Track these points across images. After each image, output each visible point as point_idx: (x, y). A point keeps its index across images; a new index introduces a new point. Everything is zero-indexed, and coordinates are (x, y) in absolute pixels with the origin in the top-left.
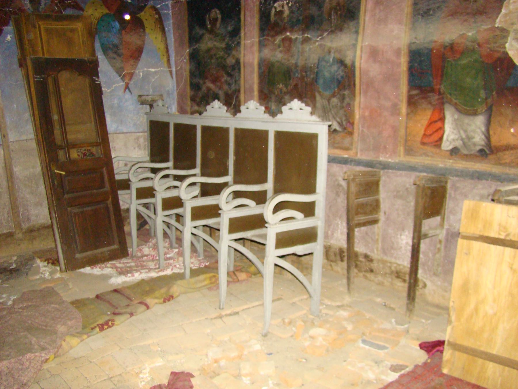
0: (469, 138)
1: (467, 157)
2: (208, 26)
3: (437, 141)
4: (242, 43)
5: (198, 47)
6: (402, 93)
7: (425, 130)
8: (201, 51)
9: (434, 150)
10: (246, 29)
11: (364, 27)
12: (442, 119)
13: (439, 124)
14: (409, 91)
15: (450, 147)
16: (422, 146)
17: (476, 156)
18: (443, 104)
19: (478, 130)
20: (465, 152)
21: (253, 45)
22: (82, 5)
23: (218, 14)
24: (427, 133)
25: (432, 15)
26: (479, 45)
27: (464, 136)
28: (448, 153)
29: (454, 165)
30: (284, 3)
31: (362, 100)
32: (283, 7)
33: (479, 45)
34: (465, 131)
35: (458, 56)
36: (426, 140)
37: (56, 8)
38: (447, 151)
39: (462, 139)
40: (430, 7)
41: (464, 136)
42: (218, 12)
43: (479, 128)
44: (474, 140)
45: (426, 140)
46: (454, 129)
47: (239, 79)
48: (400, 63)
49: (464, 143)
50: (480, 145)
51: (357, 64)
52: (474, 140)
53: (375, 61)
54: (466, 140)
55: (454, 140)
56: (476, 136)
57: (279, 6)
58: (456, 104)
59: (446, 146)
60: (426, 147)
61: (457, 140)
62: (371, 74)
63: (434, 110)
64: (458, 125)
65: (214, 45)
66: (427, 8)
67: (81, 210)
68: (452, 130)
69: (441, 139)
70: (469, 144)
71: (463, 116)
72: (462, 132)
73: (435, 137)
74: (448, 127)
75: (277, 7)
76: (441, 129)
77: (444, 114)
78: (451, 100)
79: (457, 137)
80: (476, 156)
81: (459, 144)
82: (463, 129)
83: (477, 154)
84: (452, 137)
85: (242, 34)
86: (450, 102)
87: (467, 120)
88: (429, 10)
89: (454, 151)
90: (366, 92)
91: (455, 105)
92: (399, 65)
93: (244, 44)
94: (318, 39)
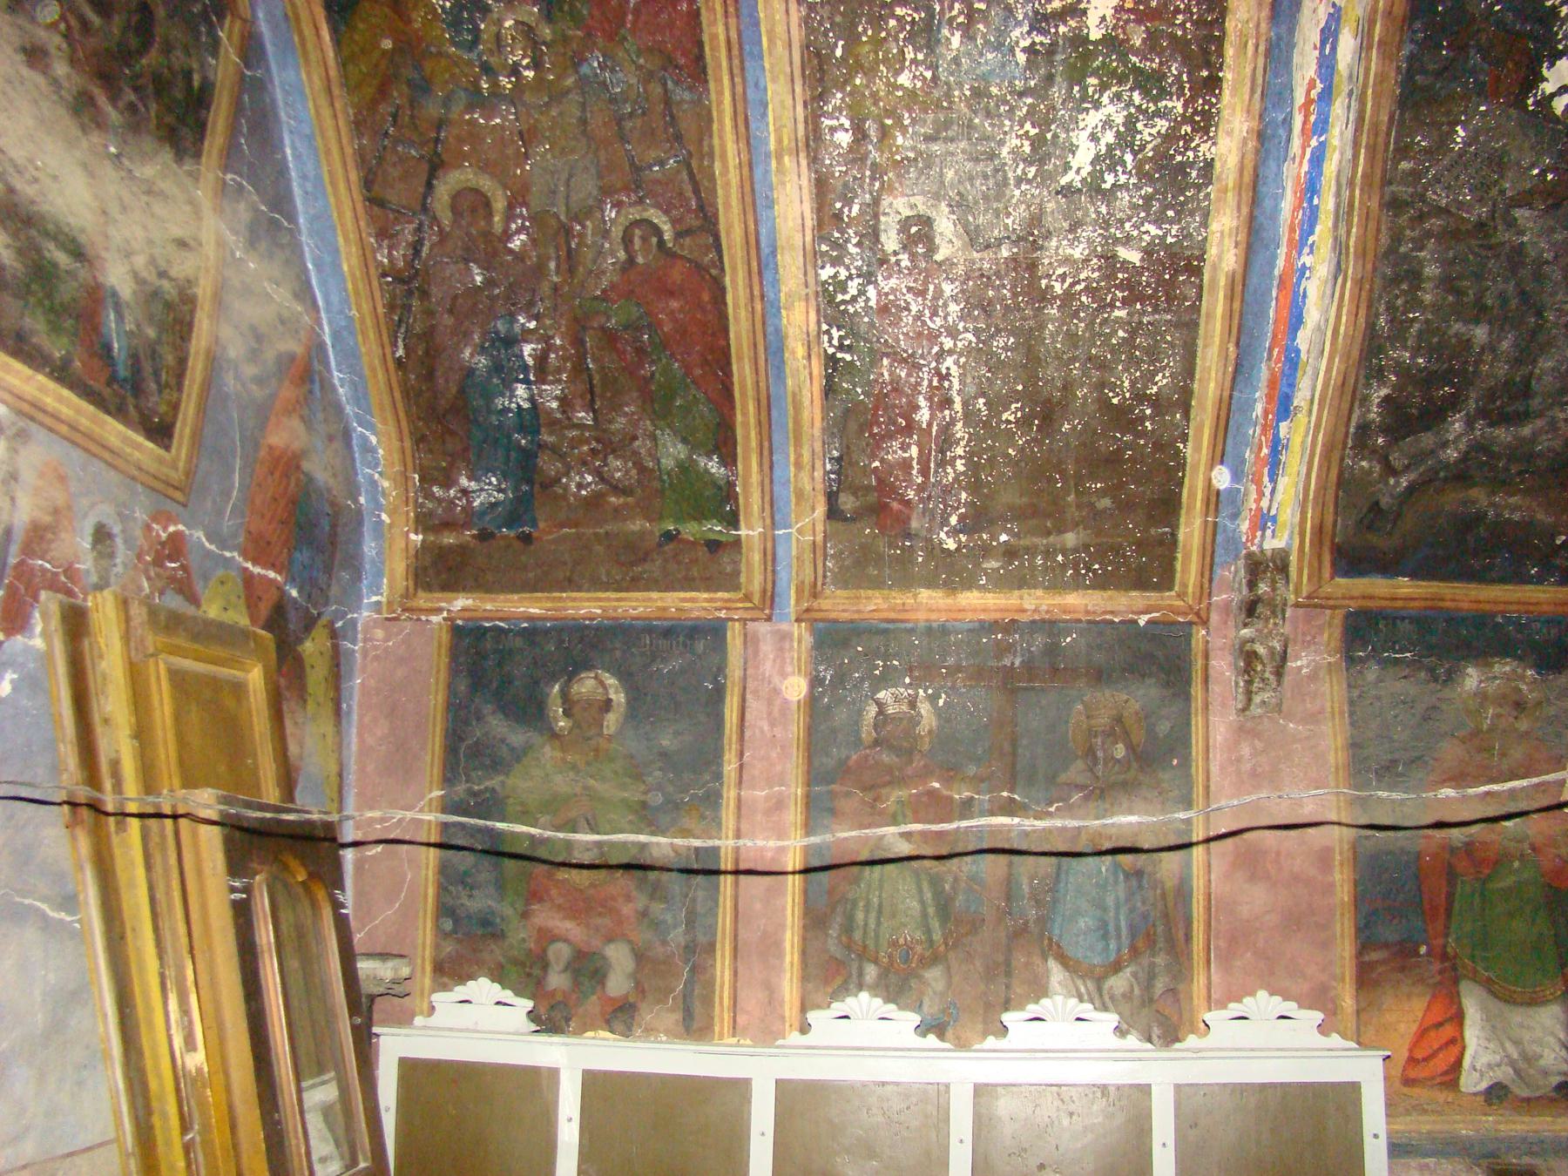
0: (1529, 1059)
1: (1528, 1104)
2: (557, 721)
3: (1445, 1073)
4: (730, 794)
5: (498, 788)
6: (1343, 958)
7: (1411, 1050)
8: (511, 801)
9: (1442, 1096)
10: (747, 754)
11: (1207, 788)
12: (1459, 1018)
13: (1448, 1031)
14: (1360, 954)
15: (1484, 1085)
16: (1406, 1090)
17: (1552, 1100)
18: (1456, 981)
19: (1552, 1040)
20: (1524, 1093)
21: (779, 805)
22: (199, 586)
23: (611, 691)
24: (1419, 1055)
25: (1402, 775)
26: (1534, 849)
27: (1515, 1056)
28: (1481, 1099)
29: (1502, 1127)
30: (917, 694)
31: (1215, 978)
32: (913, 704)
33: (1534, 849)
34: (1517, 1043)
35: (1487, 871)
36: (1415, 1073)
37: (146, 584)
38: (1475, 1094)
39: (1512, 1063)
40: (1397, 756)
41: (1515, 1056)
42: (611, 681)
43: (1553, 1034)
44: (1542, 1062)
45: (1415, 1073)
46: (1488, 1040)
47: (713, 911)
48: (1332, 885)
49: (1517, 1072)
50: (1560, 1074)
51: (1198, 885)
52: (1542, 1062)
53: (1252, 878)
54: (1522, 1065)
55: (1490, 1066)
56: (1546, 1051)
57: (897, 700)
58: (1489, 980)
59: (1472, 1081)
60: (1415, 1091)
61: (1499, 1065)
62: (1244, 911)
63: (1434, 996)
64: (1495, 1030)
65: (586, 788)
66: (1389, 757)
67: (1231, 185)
68: (1484, 1043)
69: (1458, 1063)
70: (1532, 1071)
71: (1506, 1008)
72: (1508, 1045)
73: (1441, 1063)
74: (1473, 1035)
75: (890, 701)
76: (1457, 1041)
77: (1460, 1003)
78: (1475, 972)
79: (1498, 1058)
80: (1552, 1100)
81: (1504, 1074)
82: (1510, 1039)
83: (1553, 1094)
84: (1484, 1059)
85: (730, 767)
86: (1474, 977)
87: (1516, 1016)
88: (1394, 762)
89: (1496, 1094)
90: (1227, 959)
91: (1488, 985)
92: (1329, 888)
93: (739, 799)
94: (1052, 809)
